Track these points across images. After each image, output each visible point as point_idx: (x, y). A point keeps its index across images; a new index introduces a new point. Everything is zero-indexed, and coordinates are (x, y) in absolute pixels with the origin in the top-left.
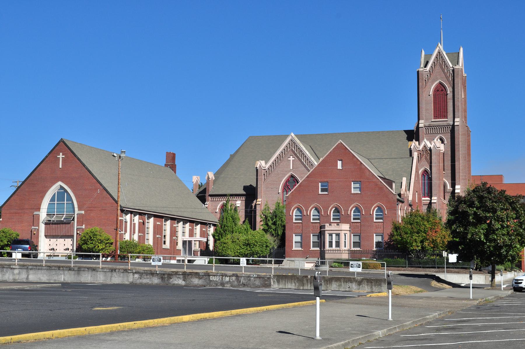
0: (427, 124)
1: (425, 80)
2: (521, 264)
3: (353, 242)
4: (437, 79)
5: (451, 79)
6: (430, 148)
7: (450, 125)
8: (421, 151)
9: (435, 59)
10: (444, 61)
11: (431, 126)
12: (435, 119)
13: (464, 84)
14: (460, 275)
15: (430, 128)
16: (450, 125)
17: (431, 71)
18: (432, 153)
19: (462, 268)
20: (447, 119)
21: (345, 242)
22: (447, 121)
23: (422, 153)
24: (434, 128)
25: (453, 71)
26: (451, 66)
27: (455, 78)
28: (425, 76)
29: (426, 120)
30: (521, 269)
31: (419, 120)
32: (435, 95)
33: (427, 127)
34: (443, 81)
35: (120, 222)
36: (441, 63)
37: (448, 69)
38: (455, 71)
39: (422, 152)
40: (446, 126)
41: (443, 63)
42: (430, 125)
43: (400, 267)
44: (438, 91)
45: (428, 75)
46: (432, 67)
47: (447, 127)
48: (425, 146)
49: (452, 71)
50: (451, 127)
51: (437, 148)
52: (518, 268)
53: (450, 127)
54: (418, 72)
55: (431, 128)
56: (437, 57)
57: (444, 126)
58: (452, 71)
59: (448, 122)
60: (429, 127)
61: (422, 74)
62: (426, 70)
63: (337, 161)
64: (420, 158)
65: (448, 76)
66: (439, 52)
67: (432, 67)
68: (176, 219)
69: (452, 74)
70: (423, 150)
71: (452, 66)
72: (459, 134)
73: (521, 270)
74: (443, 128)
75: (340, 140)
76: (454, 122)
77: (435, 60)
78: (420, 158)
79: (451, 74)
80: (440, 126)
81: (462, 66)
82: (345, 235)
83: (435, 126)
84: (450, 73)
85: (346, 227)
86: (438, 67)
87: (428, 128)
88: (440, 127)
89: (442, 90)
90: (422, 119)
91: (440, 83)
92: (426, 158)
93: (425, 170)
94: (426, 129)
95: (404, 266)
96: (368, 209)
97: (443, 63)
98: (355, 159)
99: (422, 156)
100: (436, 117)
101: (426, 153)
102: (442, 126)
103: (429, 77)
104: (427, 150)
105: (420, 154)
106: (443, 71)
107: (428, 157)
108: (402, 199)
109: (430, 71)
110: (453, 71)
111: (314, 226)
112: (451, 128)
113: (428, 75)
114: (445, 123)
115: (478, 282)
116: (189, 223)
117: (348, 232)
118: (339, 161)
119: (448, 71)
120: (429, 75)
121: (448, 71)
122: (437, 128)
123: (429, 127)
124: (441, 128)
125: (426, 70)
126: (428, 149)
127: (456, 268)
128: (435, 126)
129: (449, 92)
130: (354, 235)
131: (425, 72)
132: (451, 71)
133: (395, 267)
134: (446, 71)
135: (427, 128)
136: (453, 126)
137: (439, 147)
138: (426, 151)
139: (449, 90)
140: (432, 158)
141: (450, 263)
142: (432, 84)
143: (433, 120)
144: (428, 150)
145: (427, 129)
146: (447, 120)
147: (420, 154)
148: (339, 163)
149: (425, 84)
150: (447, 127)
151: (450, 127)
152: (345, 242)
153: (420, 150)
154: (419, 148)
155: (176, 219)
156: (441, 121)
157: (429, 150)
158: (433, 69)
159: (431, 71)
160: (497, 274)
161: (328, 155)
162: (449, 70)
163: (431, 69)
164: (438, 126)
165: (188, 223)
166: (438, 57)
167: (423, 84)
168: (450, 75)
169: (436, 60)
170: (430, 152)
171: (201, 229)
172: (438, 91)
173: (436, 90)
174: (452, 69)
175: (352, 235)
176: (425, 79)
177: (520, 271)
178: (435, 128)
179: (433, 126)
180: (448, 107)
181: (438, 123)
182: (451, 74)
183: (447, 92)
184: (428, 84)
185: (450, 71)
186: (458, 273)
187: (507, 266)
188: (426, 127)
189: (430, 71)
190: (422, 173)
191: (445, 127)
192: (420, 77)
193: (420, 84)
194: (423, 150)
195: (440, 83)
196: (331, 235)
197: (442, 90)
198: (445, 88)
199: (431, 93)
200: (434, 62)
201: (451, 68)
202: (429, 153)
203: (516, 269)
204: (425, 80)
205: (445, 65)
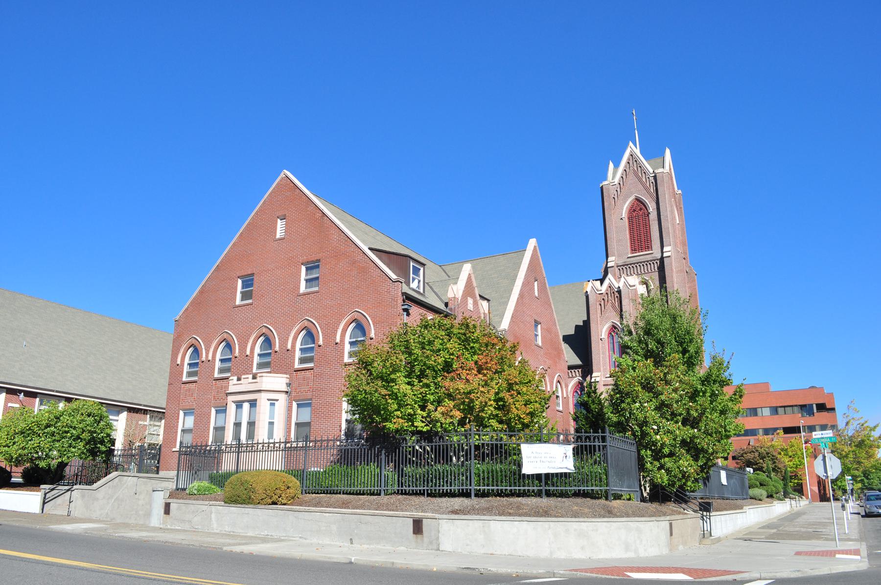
0: (620, 262)
1: (614, 198)
2: (802, 488)
3: (297, 424)
4: (632, 194)
5: (652, 191)
6: (619, 287)
7: (658, 260)
8: (604, 295)
9: (626, 166)
10: (640, 167)
11: (627, 265)
12: (633, 253)
13: (678, 204)
14: (546, 525)
15: (626, 268)
16: (658, 260)
17: (621, 183)
18: (622, 295)
19: (577, 494)
20: (652, 250)
21: (271, 424)
22: (652, 253)
23: (606, 298)
24: (633, 267)
25: (655, 177)
26: (651, 171)
27: (658, 188)
28: (613, 192)
29: (619, 256)
30: (803, 495)
31: (607, 257)
32: (630, 219)
33: (621, 266)
34: (641, 195)
35: (552, 476)
36: (636, 170)
37: (647, 177)
38: (657, 177)
39: (606, 296)
40: (651, 261)
41: (639, 169)
42: (625, 262)
43: (363, 494)
44: (634, 211)
45: (617, 191)
46: (622, 177)
47: (653, 263)
48: (610, 287)
49: (653, 178)
50: (658, 262)
51: (631, 286)
52: (797, 494)
53: (657, 262)
54: (602, 188)
55: (627, 267)
56: (628, 163)
57: (648, 261)
58: (653, 178)
59: (653, 255)
60: (623, 265)
61: (608, 189)
62: (614, 182)
63: (277, 221)
64: (603, 307)
65: (649, 186)
66: (631, 155)
67: (622, 177)
68: (38, 395)
69: (654, 183)
70: (607, 293)
71: (653, 171)
72: (672, 270)
73: (803, 497)
74: (646, 264)
75: (285, 171)
76: (662, 253)
77: (626, 166)
78: (603, 307)
79: (652, 183)
80: (641, 263)
81: (670, 169)
82: (272, 405)
83: (634, 264)
84: (651, 182)
85: (277, 381)
86: (631, 176)
87: (622, 269)
88: (641, 265)
89: (641, 209)
90: (613, 256)
91: (638, 200)
92: (613, 306)
93: (613, 326)
94: (619, 269)
95: (407, 488)
96: (330, 334)
97: (639, 169)
98: (312, 207)
99: (606, 303)
100: (634, 250)
101: (613, 296)
102: (644, 262)
103: (619, 193)
104: (613, 293)
105: (603, 299)
106: (640, 180)
107: (617, 303)
108: (451, 309)
109: (619, 184)
110: (655, 177)
111: (218, 388)
112: (658, 263)
113: (617, 191)
114: (649, 258)
115: (627, 548)
116: (125, 413)
117: (282, 398)
118: (281, 220)
119: (648, 179)
120: (619, 190)
121: (648, 179)
122: (636, 266)
123: (623, 265)
124: (643, 265)
125: (614, 182)
126: (616, 290)
127: (549, 494)
128: (633, 264)
129: (651, 210)
130: (299, 406)
131: (612, 185)
132: (652, 179)
133: (350, 494)
134: (644, 180)
135: (621, 268)
136: (662, 260)
137: (634, 284)
138: (613, 295)
139: (652, 207)
140: (623, 304)
141: (528, 475)
142: (625, 203)
143: (630, 255)
144: (615, 292)
145: (621, 270)
146: (651, 252)
147: (603, 299)
148: (280, 225)
149: (613, 203)
150: (653, 263)
151: (657, 262)
152: (271, 424)
153: (602, 294)
154: (601, 290)
155: (149, 413)
156: (642, 256)
157: (617, 292)
158: (624, 180)
159: (621, 183)
160: (742, 508)
161: (260, 210)
162: (648, 178)
163: (621, 181)
164: (637, 263)
165: (125, 413)
166: (631, 162)
167: (610, 204)
168: (651, 184)
169: (628, 167)
170: (618, 295)
171: (128, 426)
172: (634, 211)
173: (632, 210)
174: (653, 175)
175: (295, 404)
176: (613, 196)
177: (801, 498)
178: (634, 266)
179: (631, 264)
180: (652, 233)
181: (638, 258)
182: (652, 183)
183: (648, 211)
184: (618, 204)
185: (650, 178)
186: (546, 513)
187: (774, 489)
188: (619, 268)
189: (619, 184)
190: (609, 330)
191: (650, 264)
192: (604, 194)
193: (606, 204)
194: (607, 293)
195: (638, 200)
196: (239, 405)
197: (641, 209)
198: (645, 206)
199: (623, 216)
200: (625, 170)
201: (651, 174)
202: (617, 297)
203: (794, 495)
204: (614, 198)
205: (643, 172)
